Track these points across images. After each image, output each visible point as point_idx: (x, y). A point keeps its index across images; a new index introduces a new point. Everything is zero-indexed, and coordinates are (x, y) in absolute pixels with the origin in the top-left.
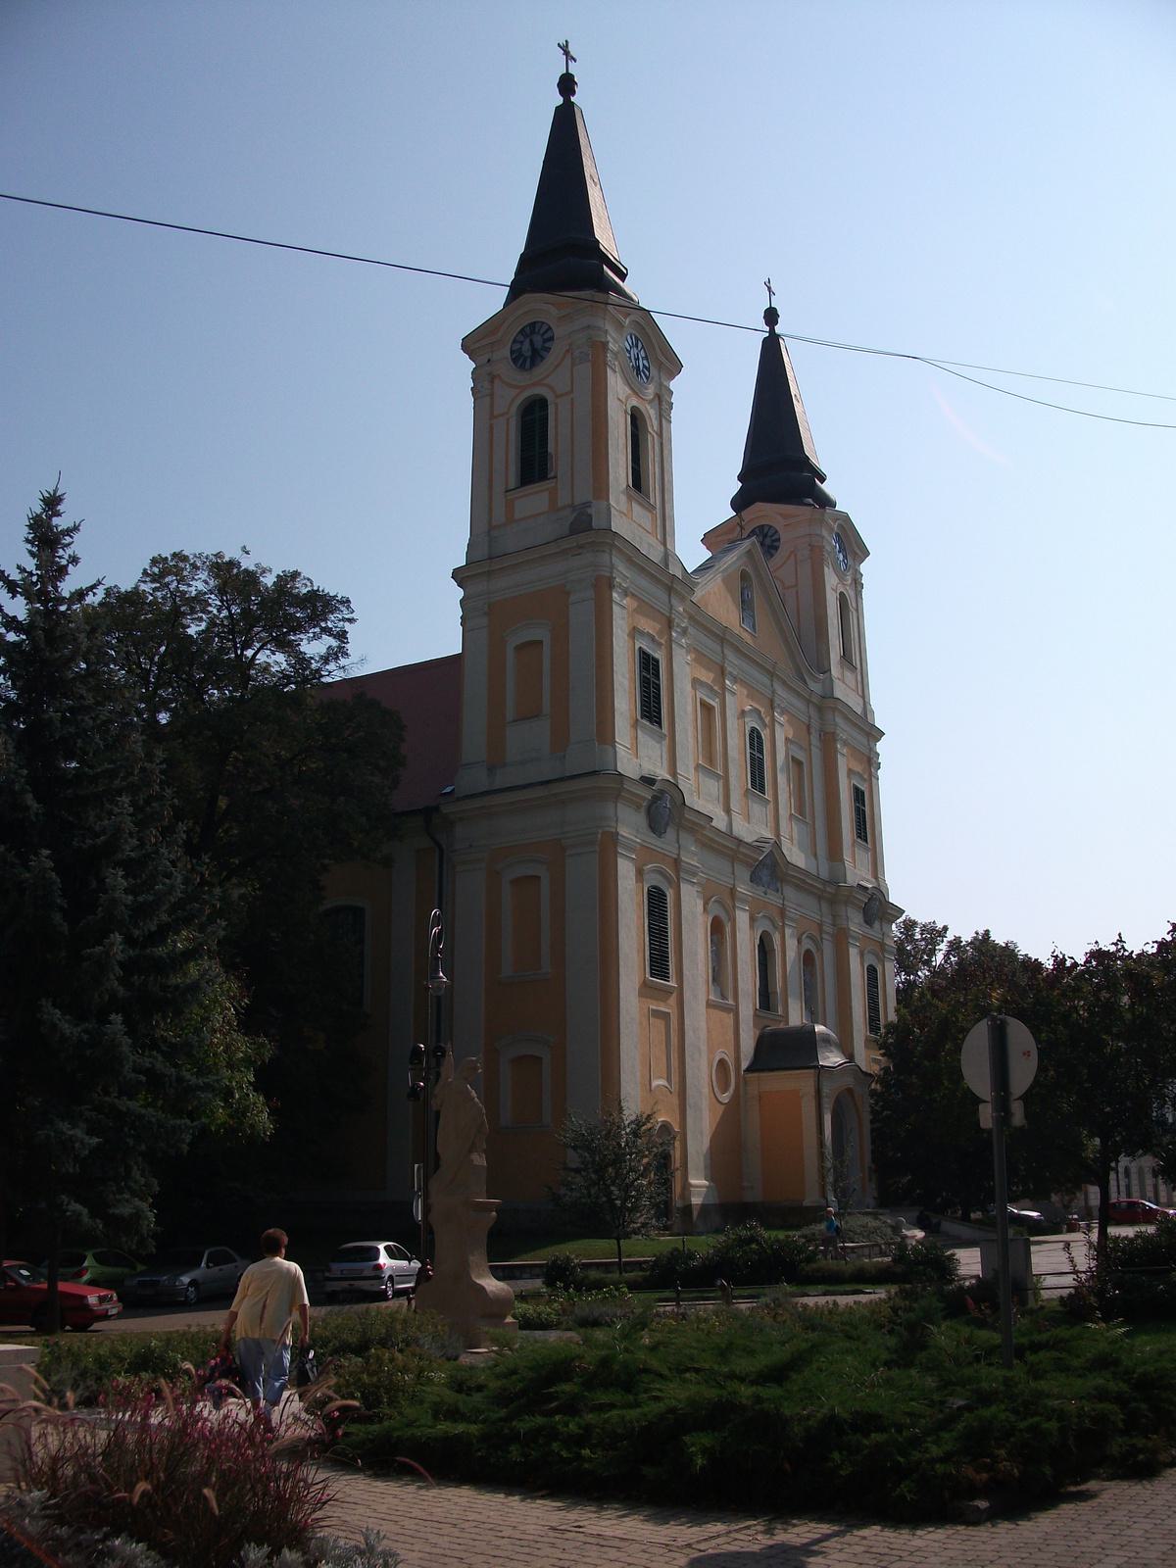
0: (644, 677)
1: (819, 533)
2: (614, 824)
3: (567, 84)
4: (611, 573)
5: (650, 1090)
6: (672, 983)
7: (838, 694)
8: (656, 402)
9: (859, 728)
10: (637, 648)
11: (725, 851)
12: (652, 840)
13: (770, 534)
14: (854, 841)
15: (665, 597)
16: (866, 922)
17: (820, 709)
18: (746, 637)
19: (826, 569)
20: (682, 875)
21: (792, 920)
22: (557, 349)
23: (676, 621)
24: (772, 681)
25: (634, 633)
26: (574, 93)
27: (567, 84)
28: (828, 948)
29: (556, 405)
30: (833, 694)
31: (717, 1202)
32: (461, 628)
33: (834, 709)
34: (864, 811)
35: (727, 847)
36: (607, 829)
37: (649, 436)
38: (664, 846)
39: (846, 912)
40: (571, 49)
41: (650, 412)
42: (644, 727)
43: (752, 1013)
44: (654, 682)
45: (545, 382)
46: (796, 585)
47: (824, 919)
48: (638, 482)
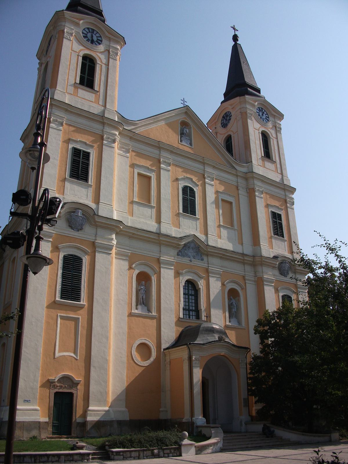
0: (274, 221)
1: (245, 107)
2: (261, 274)
3: (235, 38)
4: (254, 186)
5: (54, 358)
6: (154, 314)
7: (255, 171)
8: (274, 128)
9: (279, 187)
10: (270, 211)
11: (239, 260)
12: (282, 278)
13: (228, 115)
14: (271, 237)
15: (283, 193)
16: (281, 274)
17: (246, 179)
18: (189, 150)
19: (249, 121)
20: (247, 282)
21: (248, 280)
22: (233, 118)
23: (288, 199)
24: (237, 179)
25: (267, 206)
26: (238, 40)
27: (235, 38)
28: (251, 288)
29: (234, 136)
30: (104, 115)
31: (128, 419)
32: (21, 163)
33: (253, 178)
34: (281, 224)
35: (154, 239)
36: (259, 276)
37: (271, 139)
38: (80, 235)
39: (262, 269)
40: (236, 27)
41: (271, 133)
42: (276, 238)
43: (175, 320)
44: (279, 222)
45: (231, 130)
46: (237, 131)
47: (246, 273)
48: (267, 154)
